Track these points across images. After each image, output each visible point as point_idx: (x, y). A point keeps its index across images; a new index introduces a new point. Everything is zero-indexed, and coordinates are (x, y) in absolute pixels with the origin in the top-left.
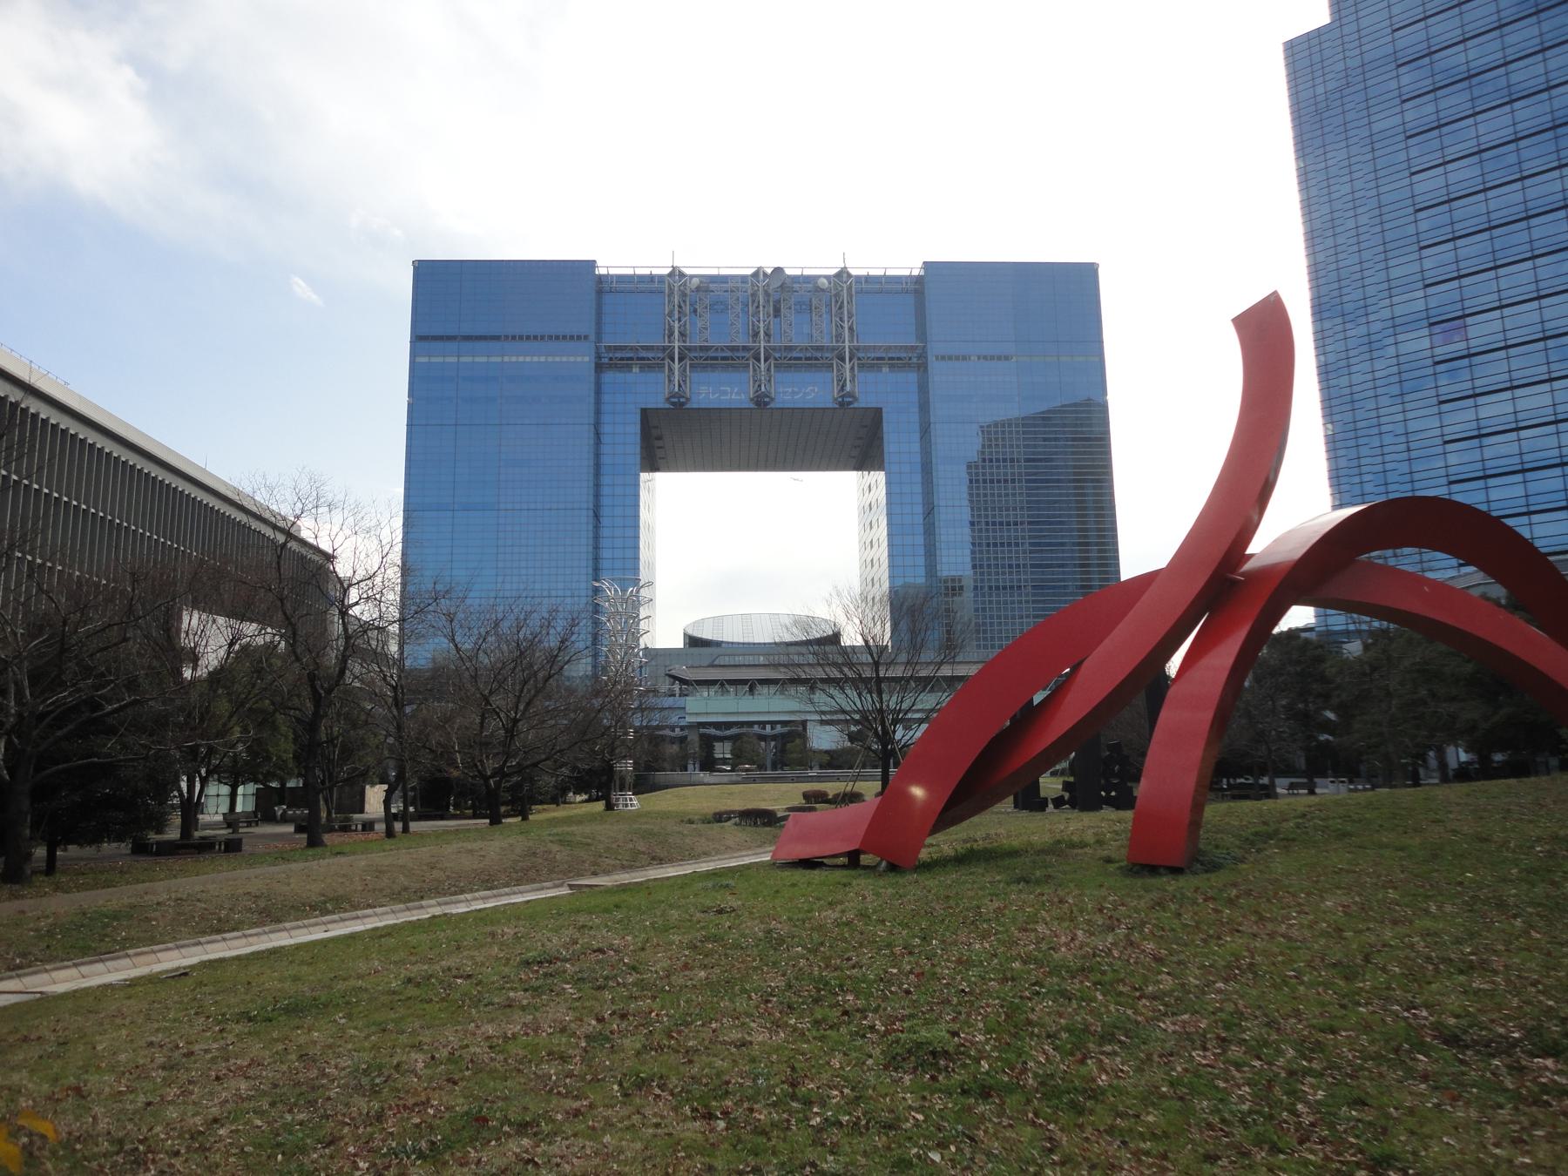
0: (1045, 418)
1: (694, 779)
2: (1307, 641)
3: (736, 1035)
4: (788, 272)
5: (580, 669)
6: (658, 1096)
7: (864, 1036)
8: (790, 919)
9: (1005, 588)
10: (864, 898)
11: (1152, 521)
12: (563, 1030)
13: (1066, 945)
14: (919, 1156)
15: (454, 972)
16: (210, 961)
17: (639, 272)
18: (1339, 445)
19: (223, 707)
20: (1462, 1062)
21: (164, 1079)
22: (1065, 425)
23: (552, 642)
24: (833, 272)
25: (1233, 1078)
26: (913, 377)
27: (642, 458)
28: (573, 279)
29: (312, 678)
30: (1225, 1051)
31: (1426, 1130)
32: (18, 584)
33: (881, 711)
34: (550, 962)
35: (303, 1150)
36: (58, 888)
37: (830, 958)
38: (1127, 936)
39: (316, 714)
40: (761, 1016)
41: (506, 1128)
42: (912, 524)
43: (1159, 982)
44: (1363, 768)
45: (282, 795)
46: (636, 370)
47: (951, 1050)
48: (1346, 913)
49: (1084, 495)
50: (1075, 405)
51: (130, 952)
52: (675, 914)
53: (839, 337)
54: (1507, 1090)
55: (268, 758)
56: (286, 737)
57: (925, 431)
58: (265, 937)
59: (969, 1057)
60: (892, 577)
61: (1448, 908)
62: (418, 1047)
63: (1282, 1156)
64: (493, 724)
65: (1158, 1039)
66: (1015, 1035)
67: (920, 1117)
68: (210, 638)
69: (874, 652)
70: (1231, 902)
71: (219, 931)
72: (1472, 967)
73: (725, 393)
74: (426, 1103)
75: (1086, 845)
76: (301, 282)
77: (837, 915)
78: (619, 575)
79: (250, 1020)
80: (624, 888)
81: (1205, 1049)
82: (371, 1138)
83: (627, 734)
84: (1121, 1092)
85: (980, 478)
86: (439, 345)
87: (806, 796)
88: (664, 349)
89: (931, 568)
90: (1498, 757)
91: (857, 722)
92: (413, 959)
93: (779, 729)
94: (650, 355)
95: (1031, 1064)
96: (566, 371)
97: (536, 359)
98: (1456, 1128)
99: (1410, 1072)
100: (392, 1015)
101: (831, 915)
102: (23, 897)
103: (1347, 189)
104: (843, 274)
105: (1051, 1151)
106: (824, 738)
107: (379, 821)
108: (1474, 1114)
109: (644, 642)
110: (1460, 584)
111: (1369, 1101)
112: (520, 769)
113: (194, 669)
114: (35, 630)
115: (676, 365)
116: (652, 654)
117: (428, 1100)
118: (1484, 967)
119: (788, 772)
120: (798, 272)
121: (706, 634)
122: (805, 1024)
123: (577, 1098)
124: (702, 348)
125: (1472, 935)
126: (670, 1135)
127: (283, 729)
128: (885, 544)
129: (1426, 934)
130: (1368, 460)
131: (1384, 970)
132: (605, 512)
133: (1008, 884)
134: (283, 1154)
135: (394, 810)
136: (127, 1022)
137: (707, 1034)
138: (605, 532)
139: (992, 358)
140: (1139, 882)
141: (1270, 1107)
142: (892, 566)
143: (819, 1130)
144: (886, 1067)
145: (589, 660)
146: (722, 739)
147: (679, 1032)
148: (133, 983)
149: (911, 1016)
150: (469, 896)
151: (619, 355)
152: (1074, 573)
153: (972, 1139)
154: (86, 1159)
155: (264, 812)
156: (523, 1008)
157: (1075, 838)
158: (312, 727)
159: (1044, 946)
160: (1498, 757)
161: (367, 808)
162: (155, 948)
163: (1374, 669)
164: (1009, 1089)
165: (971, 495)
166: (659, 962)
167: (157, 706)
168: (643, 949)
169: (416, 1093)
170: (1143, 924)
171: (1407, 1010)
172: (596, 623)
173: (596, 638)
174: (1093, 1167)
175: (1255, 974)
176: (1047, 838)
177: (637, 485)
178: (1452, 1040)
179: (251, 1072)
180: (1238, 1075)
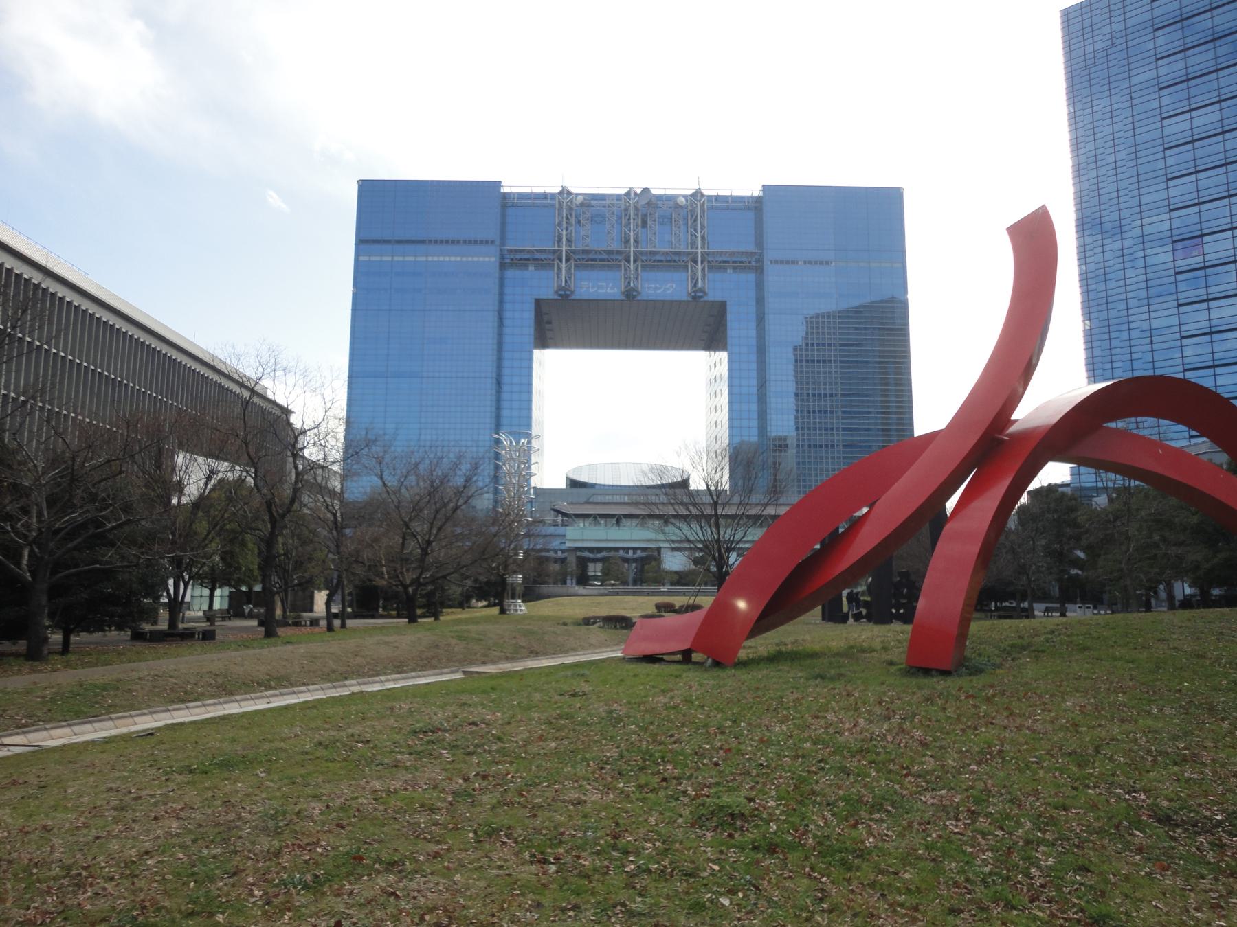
0: (857, 312)
1: (571, 591)
2: (1063, 494)
3: (574, 795)
4: (654, 192)
5: (484, 502)
6: (504, 843)
7: (677, 799)
8: (629, 703)
9: (821, 446)
10: (691, 687)
11: (938, 396)
12: (435, 787)
13: (849, 730)
14: (711, 901)
15: (356, 738)
16: (174, 725)
17: (536, 190)
18: (1095, 338)
19: (202, 527)
20: (1172, 838)
21: (114, 818)
22: (873, 318)
23: (459, 481)
24: (689, 192)
25: (979, 844)
26: (751, 277)
27: (536, 339)
28: (484, 193)
29: (269, 505)
30: (973, 822)
31: (1138, 895)
32: (40, 429)
33: (718, 541)
34: (433, 732)
35: (212, 879)
36: (68, 665)
37: (656, 735)
38: (900, 724)
39: (272, 533)
40: (596, 780)
41: (377, 866)
42: (749, 394)
43: (923, 763)
44: (1106, 597)
45: (249, 597)
46: (531, 268)
47: (747, 813)
48: (1082, 712)
49: (887, 374)
50: (881, 301)
51: (113, 716)
52: (537, 696)
53: (694, 244)
54: (1209, 863)
55: (239, 568)
56: (253, 552)
57: (761, 319)
58: (219, 707)
59: (761, 819)
60: (731, 436)
61: (1167, 711)
62: (316, 797)
63: (1015, 912)
64: (412, 544)
65: (918, 810)
66: (801, 803)
67: (716, 868)
68: (195, 475)
69: (715, 495)
70: (988, 700)
71: (184, 701)
72: (1185, 760)
73: (602, 287)
74: (317, 844)
75: (874, 650)
76: (275, 195)
77: (666, 700)
78: (515, 430)
79: (191, 772)
80: (504, 675)
81: (957, 820)
82: (267, 871)
83: (517, 554)
84: (885, 853)
85: (803, 359)
86: (377, 247)
87: (658, 606)
88: (554, 252)
89: (762, 428)
90: (1216, 592)
91: (701, 550)
92: (327, 726)
93: (639, 553)
94: (543, 256)
95: (812, 827)
96: (474, 268)
97: (453, 259)
98: (1164, 894)
99: (1127, 846)
100: (303, 771)
101: (663, 700)
102: (40, 671)
103: (1109, 130)
104: (697, 194)
105: (821, 900)
106: (674, 562)
107: (322, 618)
108: (1179, 882)
109: (536, 482)
110: (1193, 451)
111: (1092, 868)
112: (433, 580)
113: (179, 499)
114: (53, 462)
115: (564, 265)
116: (540, 492)
117: (319, 840)
118: (1195, 758)
119: (645, 588)
120: (661, 192)
121: (584, 478)
122: (631, 788)
123: (439, 843)
124: (584, 252)
125: (1186, 734)
126: (509, 875)
127: (250, 545)
128: (727, 409)
129: (1148, 731)
130: (1118, 351)
131: (1111, 759)
132: (506, 380)
133: (807, 679)
134: (196, 882)
135: (334, 610)
136: (95, 771)
137: (550, 794)
138: (505, 396)
139: (816, 263)
140: (914, 681)
141: (1008, 871)
142: (731, 427)
143: (633, 875)
144: (693, 826)
145: (491, 496)
146: (594, 560)
147: (529, 791)
148: (110, 740)
149: (718, 784)
150: (383, 678)
151: (518, 256)
152: (877, 436)
153: (757, 888)
154: (39, 881)
155: (235, 610)
156: (407, 768)
157: (865, 644)
158: (270, 542)
159: (831, 730)
160: (1216, 592)
161: (316, 608)
162: (133, 713)
163: (1116, 518)
164: (791, 847)
165: (796, 372)
166: (521, 734)
167: (148, 525)
168: (509, 723)
169: (310, 835)
170: (914, 715)
171: (1129, 793)
172: (497, 468)
173: (496, 479)
174: (855, 915)
175: (1003, 759)
176: (843, 644)
177: (530, 359)
178: (1166, 820)
179: (182, 814)
180: (983, 842)
